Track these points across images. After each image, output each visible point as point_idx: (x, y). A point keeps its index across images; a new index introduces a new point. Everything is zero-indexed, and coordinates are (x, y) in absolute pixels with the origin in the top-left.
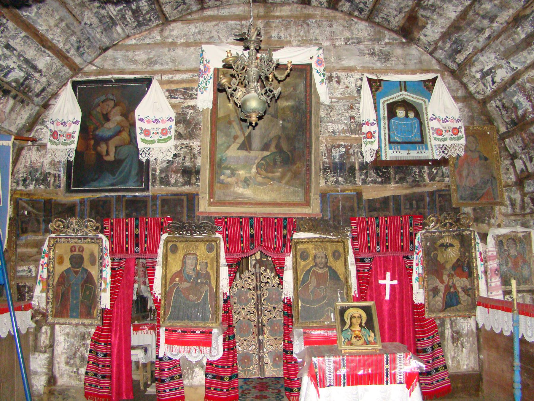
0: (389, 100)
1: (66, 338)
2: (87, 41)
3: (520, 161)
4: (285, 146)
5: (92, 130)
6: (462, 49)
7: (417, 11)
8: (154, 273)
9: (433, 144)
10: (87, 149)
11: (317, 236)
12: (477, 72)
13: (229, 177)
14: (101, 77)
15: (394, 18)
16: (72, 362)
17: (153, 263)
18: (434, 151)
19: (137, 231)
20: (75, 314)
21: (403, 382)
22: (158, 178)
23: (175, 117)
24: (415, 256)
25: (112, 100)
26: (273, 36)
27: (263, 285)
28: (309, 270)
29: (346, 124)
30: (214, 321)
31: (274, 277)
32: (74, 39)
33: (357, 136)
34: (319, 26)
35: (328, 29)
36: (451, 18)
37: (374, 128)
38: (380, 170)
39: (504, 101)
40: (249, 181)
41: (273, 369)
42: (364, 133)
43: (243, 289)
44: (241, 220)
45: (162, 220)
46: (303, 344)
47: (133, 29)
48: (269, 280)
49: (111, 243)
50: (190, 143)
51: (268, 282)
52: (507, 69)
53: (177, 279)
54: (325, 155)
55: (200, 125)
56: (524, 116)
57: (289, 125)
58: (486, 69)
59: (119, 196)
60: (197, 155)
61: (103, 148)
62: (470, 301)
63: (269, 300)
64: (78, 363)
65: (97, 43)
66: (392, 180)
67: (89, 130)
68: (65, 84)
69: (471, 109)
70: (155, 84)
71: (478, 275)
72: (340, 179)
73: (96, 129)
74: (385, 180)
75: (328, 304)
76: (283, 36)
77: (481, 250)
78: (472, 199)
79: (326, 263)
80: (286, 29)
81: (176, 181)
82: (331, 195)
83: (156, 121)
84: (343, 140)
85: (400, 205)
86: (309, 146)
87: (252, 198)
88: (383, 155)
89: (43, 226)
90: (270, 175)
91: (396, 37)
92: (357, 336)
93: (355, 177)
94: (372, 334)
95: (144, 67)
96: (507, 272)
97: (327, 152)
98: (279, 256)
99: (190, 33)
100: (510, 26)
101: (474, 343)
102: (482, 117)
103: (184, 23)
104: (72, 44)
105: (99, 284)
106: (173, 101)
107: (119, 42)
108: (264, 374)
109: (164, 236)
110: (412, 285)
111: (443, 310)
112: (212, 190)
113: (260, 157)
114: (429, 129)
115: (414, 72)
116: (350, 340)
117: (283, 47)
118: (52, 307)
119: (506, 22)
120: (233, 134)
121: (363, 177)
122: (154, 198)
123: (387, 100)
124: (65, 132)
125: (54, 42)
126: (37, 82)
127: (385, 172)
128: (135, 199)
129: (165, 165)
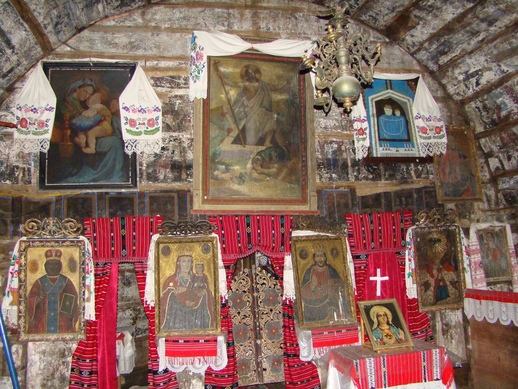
0: (377, 97)
1: (42, 356)
2: (66, 18)
3: (497, 159)
4: (280, 141)
5: (68, 118)
6: (449, 51)
7: (411, 11)
8: (145, 278)
9: (419, 141)
10: (62, 141)
11: (316, 234)
12: (460, 73)
13: (223, 173)
14: (77, 60)
15: (384, 17)
16: (49, 384)
17: (142, 267)
18: (420, 148)
19: (124, 232)
20: (52, 328)
21: (439, 378)
22: (145, 174)
23: (162, 107)
24: (407, 252)
25: (90, 85)
26: (262, 27)
27: (259, 286)
28: (309, 269)
29: (337, 120)
30: (214, 328)
31: (270, 277)
32: (55, 12)
33: (348, 132)
34: (307, 21)
35: (315, 24)
36: (446, 20)
37: (365, 125)
38: (371, 167)
39: (487, 102)
40: (244, 176)
41: (272, 374)
42: (356, 130)
43: (237, 292)
44: (237, 218)
45: (152, 220)
46: (312, 346)
47: (114, 9)
48: (265, 282)
49: (94, 246)
50: (179, 136)
51: (264, 284)
52: (497, 72)
53: (171, 284)
54: (318, 151)
55: (189, 117)
56: (507, 117)
57: (283, 119)
58: (472, 70)
59: (101, 193)
60: (187, 149)
61: (81, 139)
62: (458, 294)
63: (267, 301)
64: (57, 385)
65: (75, 21)
66: (383, 177)
67: (65, 118)
68: (33, 66)
69: (450, 110)
70: (139, 72)
71: (464, 269)
72: (334, 175)
73: (72, 117)
74: (376, 177)
75: (330, 304)
76: (271, 28)
77: (466, 244)
78: (455, 196)
79: (326, 261)
80: (275, 21)
81: (165, 176)
82: (325, 192)
83: (142, 111)
84: (335, 136)
85: (390, 202)
86: (304, 141)
87: (249, 196)
88: (374, 151)
89: (11, 228)
90: (266, 171)
91: (380, 36)
92: (387, 335)
93: (348, 174)
94: (401, 332)
95: (126, 51)
96: (489, 265)
97: (320, 148)
98: (279, 256)
99: (174, 18)
100: (510, 30)
101: (461, 334)
102: (459, 117)
103: (168, 7)
104: (51, 19)
105: (82, 292)
106: (159, 89)
107: (96, 22)
108: (263, 381)
109: (155, 237)
110: (405, 281)
111: (434, 304)
112: (206, 186)
113: (255, 152)
114: (414, 127)
115: (397, 71)
116: (382, 340)
117: (277, 39)
118: (25, 322)
119: (506, 26)
120: (226, 127)
121: (355, 174)
122: (142, 195)
123: (375, 98)
124: (36, 120)
125: (36, 13)
126: (8, 59)
127: (375, 169)
128: (119, 196)
129: (152, 159)
